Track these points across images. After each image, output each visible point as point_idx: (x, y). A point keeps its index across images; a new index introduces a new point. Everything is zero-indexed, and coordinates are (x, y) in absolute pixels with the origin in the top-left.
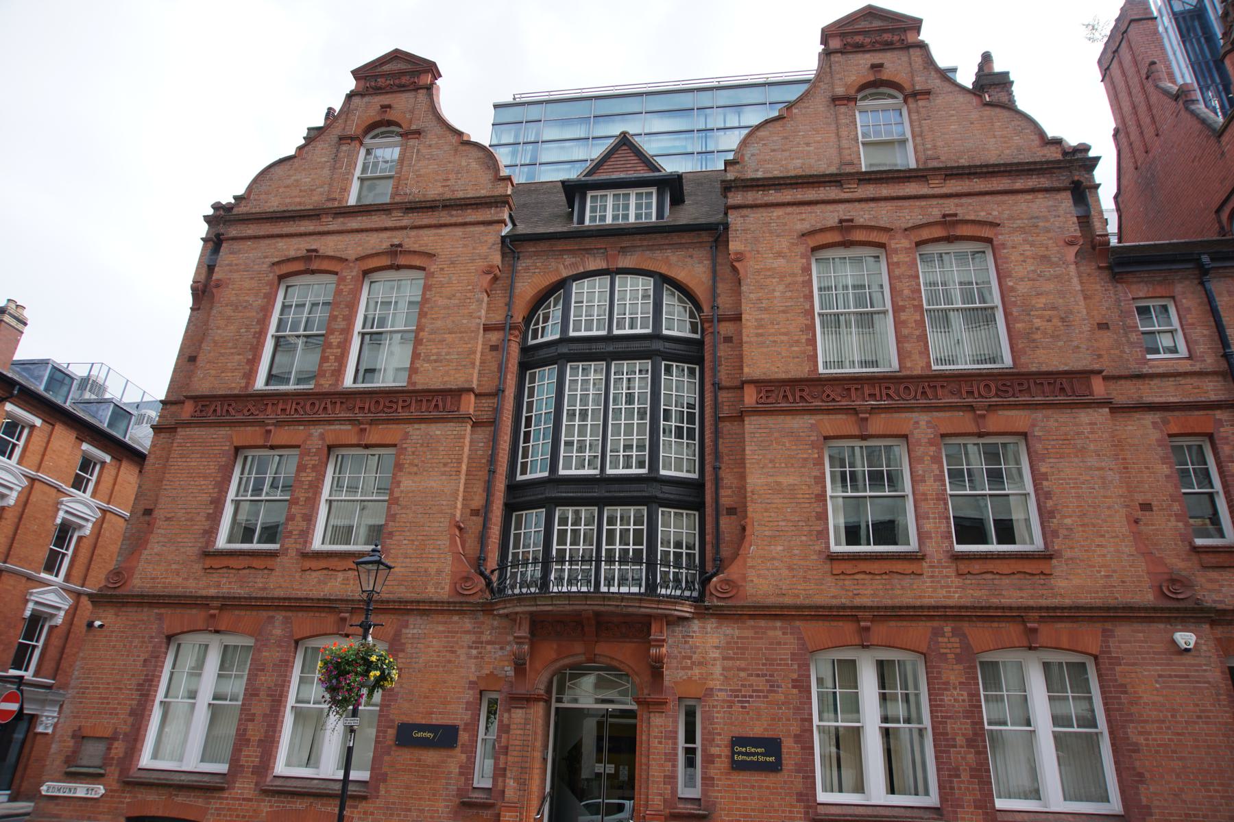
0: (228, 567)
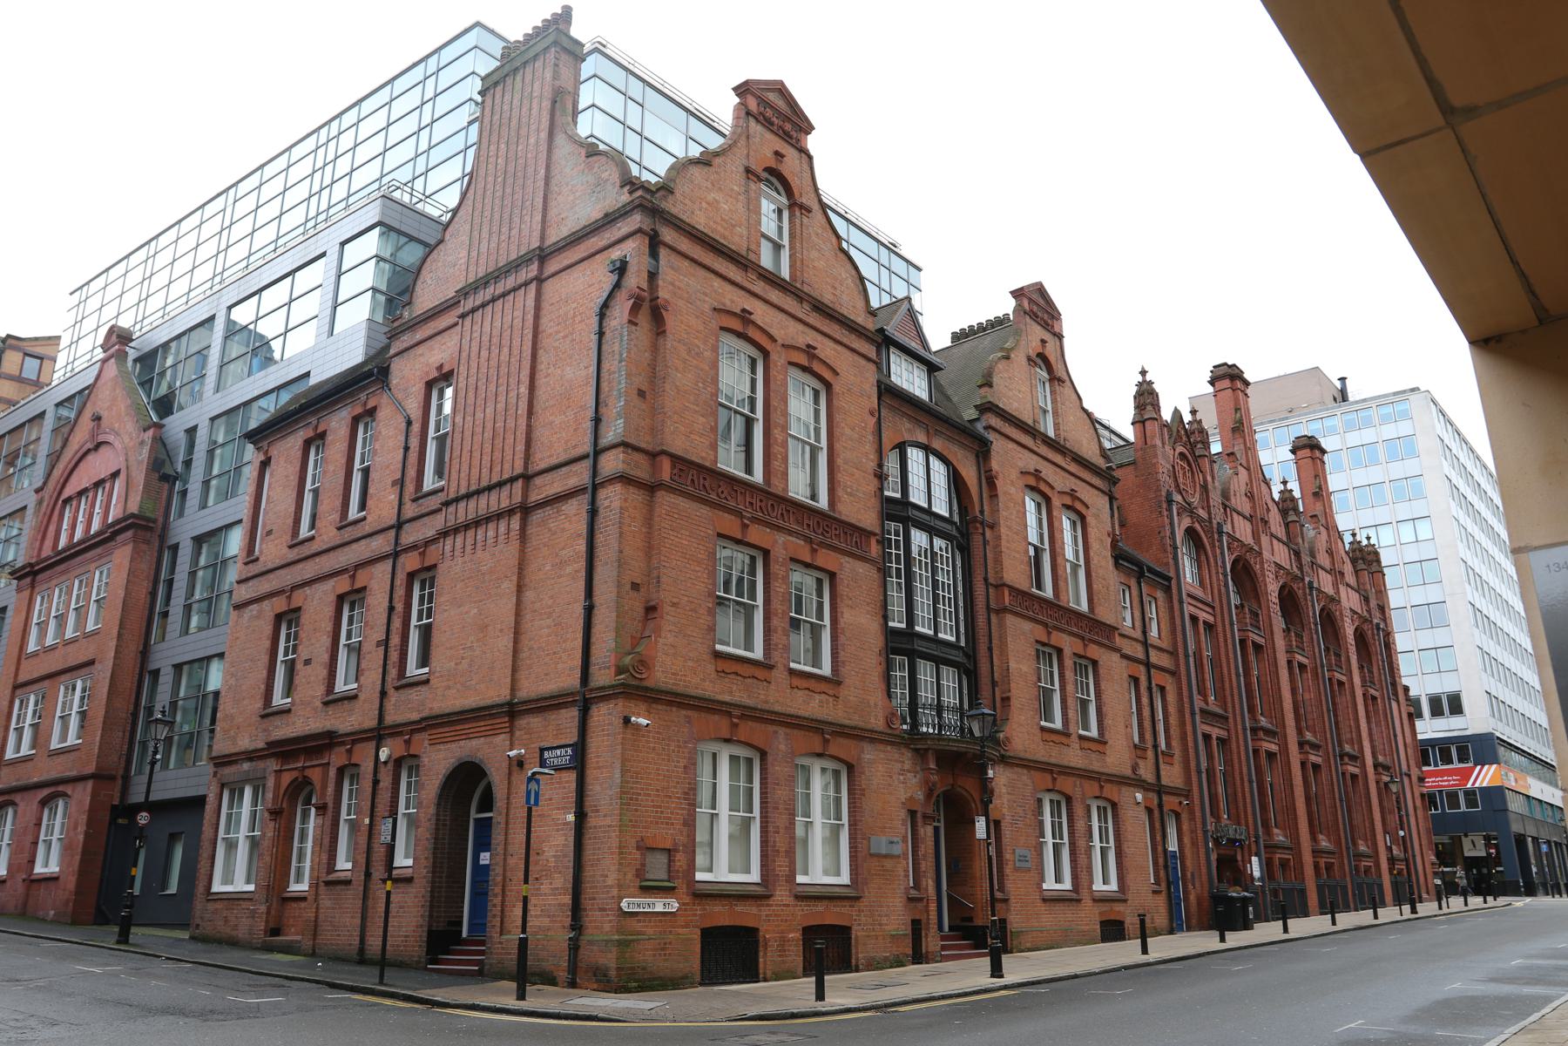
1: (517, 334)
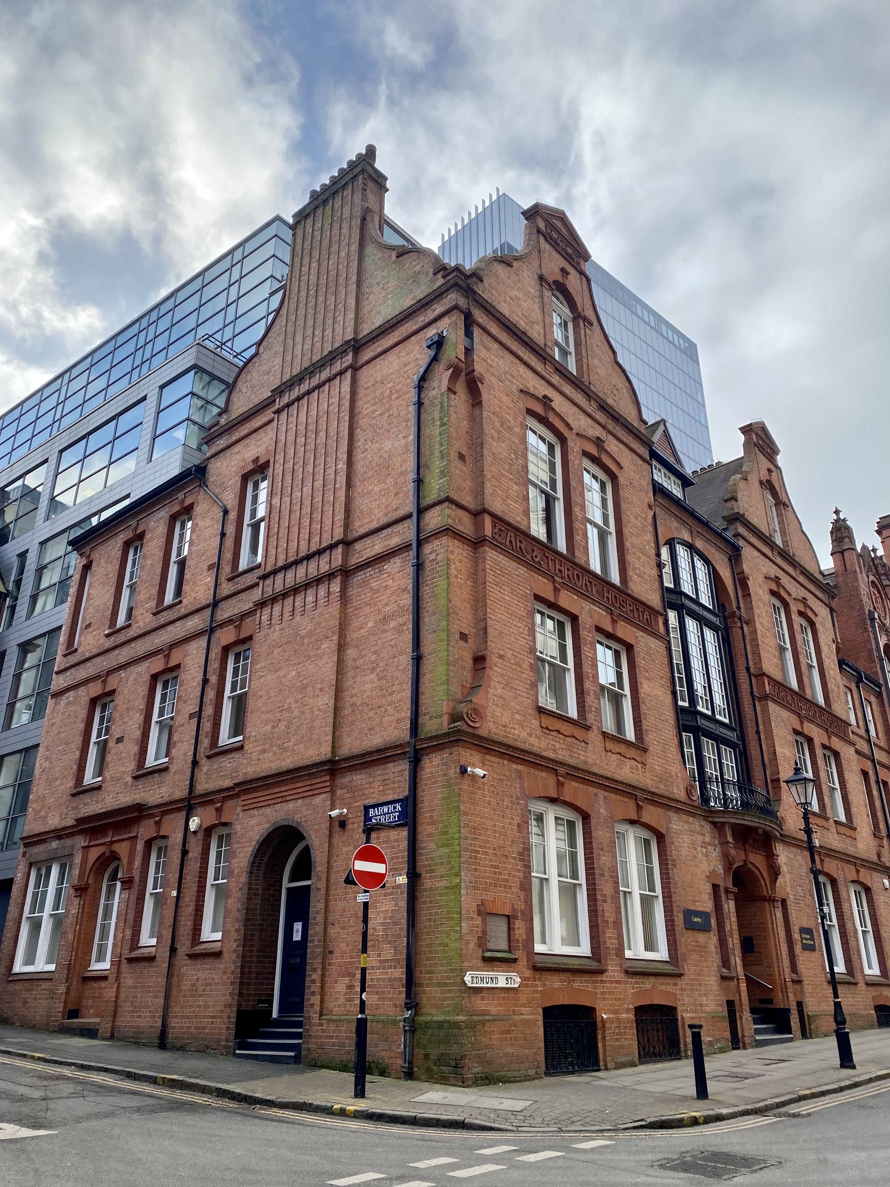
0: (558, 731)
1: (334, 417)
